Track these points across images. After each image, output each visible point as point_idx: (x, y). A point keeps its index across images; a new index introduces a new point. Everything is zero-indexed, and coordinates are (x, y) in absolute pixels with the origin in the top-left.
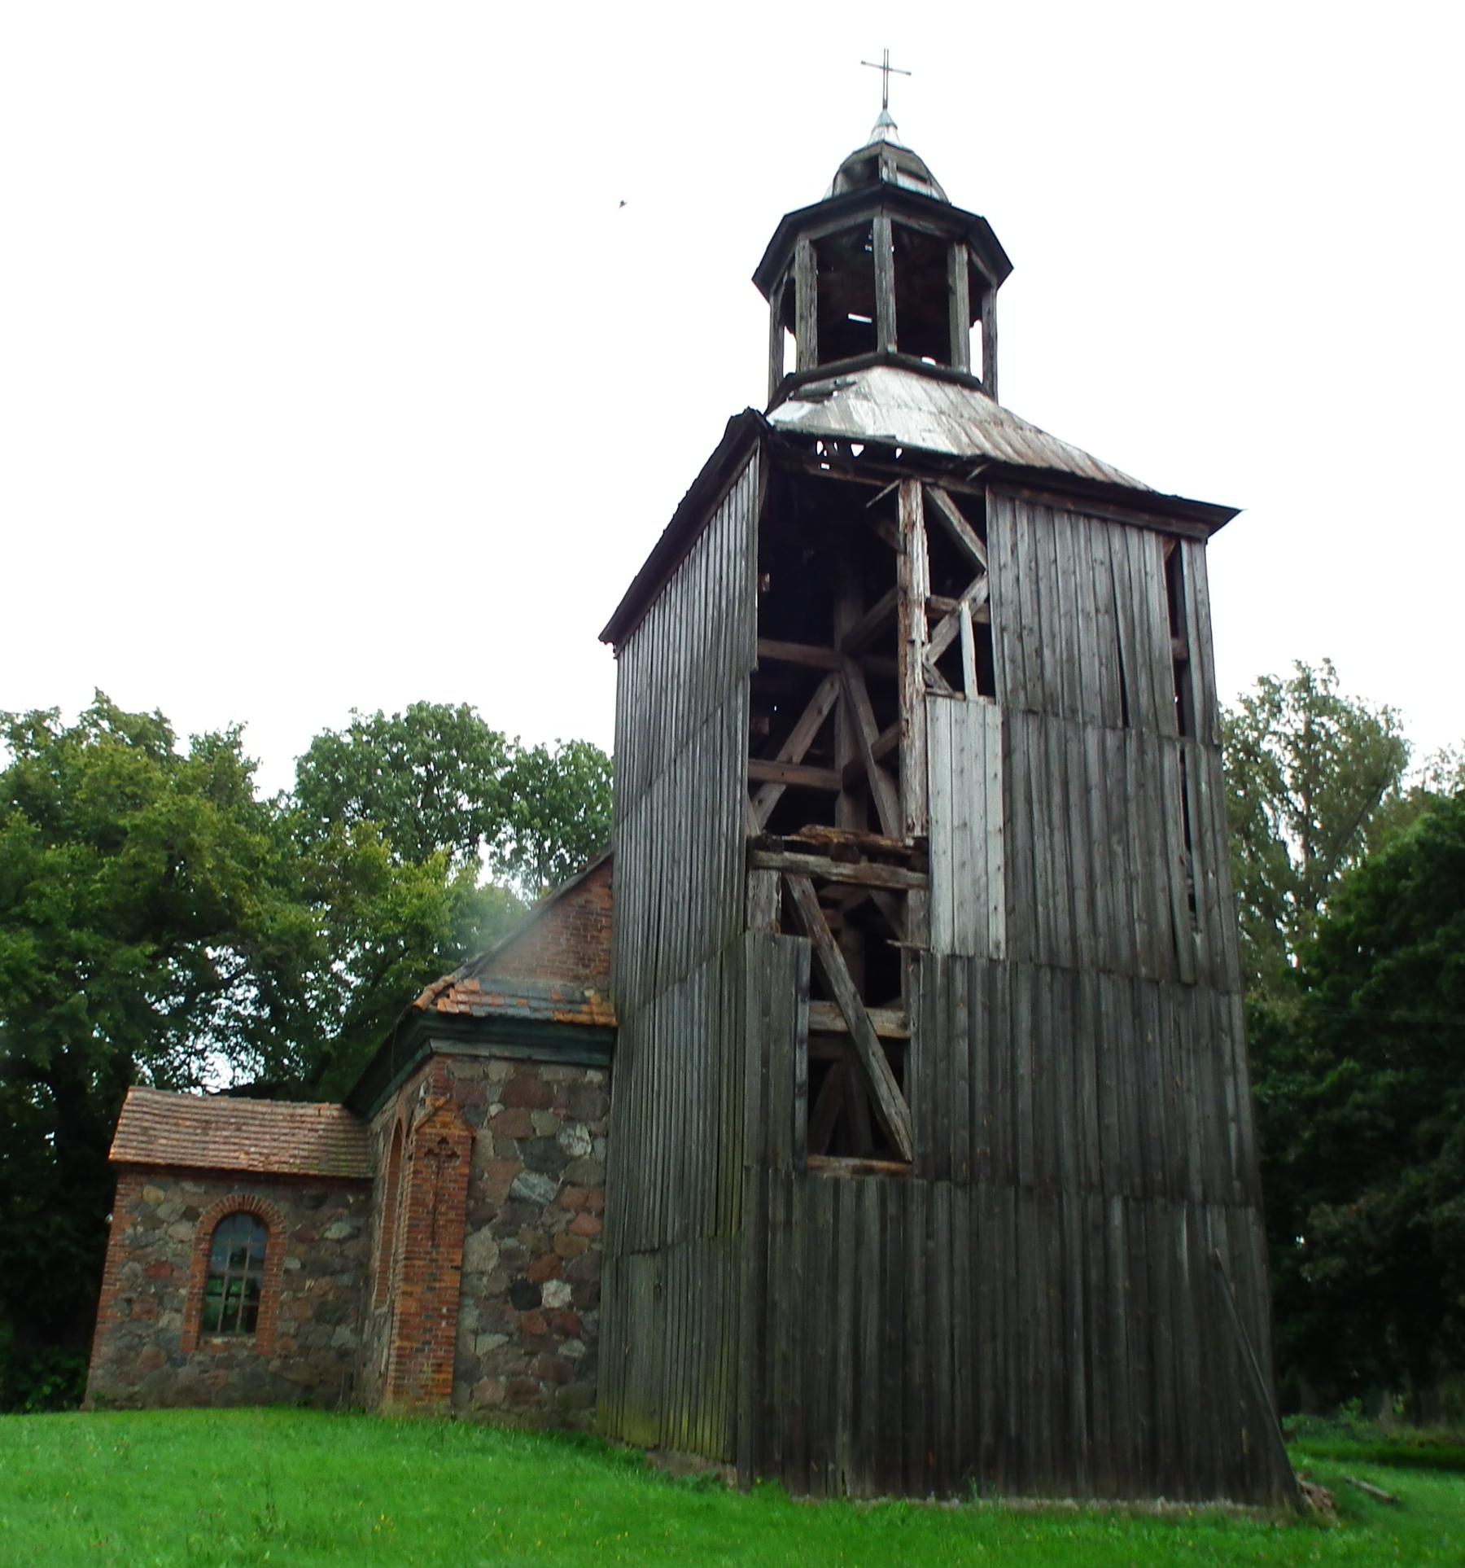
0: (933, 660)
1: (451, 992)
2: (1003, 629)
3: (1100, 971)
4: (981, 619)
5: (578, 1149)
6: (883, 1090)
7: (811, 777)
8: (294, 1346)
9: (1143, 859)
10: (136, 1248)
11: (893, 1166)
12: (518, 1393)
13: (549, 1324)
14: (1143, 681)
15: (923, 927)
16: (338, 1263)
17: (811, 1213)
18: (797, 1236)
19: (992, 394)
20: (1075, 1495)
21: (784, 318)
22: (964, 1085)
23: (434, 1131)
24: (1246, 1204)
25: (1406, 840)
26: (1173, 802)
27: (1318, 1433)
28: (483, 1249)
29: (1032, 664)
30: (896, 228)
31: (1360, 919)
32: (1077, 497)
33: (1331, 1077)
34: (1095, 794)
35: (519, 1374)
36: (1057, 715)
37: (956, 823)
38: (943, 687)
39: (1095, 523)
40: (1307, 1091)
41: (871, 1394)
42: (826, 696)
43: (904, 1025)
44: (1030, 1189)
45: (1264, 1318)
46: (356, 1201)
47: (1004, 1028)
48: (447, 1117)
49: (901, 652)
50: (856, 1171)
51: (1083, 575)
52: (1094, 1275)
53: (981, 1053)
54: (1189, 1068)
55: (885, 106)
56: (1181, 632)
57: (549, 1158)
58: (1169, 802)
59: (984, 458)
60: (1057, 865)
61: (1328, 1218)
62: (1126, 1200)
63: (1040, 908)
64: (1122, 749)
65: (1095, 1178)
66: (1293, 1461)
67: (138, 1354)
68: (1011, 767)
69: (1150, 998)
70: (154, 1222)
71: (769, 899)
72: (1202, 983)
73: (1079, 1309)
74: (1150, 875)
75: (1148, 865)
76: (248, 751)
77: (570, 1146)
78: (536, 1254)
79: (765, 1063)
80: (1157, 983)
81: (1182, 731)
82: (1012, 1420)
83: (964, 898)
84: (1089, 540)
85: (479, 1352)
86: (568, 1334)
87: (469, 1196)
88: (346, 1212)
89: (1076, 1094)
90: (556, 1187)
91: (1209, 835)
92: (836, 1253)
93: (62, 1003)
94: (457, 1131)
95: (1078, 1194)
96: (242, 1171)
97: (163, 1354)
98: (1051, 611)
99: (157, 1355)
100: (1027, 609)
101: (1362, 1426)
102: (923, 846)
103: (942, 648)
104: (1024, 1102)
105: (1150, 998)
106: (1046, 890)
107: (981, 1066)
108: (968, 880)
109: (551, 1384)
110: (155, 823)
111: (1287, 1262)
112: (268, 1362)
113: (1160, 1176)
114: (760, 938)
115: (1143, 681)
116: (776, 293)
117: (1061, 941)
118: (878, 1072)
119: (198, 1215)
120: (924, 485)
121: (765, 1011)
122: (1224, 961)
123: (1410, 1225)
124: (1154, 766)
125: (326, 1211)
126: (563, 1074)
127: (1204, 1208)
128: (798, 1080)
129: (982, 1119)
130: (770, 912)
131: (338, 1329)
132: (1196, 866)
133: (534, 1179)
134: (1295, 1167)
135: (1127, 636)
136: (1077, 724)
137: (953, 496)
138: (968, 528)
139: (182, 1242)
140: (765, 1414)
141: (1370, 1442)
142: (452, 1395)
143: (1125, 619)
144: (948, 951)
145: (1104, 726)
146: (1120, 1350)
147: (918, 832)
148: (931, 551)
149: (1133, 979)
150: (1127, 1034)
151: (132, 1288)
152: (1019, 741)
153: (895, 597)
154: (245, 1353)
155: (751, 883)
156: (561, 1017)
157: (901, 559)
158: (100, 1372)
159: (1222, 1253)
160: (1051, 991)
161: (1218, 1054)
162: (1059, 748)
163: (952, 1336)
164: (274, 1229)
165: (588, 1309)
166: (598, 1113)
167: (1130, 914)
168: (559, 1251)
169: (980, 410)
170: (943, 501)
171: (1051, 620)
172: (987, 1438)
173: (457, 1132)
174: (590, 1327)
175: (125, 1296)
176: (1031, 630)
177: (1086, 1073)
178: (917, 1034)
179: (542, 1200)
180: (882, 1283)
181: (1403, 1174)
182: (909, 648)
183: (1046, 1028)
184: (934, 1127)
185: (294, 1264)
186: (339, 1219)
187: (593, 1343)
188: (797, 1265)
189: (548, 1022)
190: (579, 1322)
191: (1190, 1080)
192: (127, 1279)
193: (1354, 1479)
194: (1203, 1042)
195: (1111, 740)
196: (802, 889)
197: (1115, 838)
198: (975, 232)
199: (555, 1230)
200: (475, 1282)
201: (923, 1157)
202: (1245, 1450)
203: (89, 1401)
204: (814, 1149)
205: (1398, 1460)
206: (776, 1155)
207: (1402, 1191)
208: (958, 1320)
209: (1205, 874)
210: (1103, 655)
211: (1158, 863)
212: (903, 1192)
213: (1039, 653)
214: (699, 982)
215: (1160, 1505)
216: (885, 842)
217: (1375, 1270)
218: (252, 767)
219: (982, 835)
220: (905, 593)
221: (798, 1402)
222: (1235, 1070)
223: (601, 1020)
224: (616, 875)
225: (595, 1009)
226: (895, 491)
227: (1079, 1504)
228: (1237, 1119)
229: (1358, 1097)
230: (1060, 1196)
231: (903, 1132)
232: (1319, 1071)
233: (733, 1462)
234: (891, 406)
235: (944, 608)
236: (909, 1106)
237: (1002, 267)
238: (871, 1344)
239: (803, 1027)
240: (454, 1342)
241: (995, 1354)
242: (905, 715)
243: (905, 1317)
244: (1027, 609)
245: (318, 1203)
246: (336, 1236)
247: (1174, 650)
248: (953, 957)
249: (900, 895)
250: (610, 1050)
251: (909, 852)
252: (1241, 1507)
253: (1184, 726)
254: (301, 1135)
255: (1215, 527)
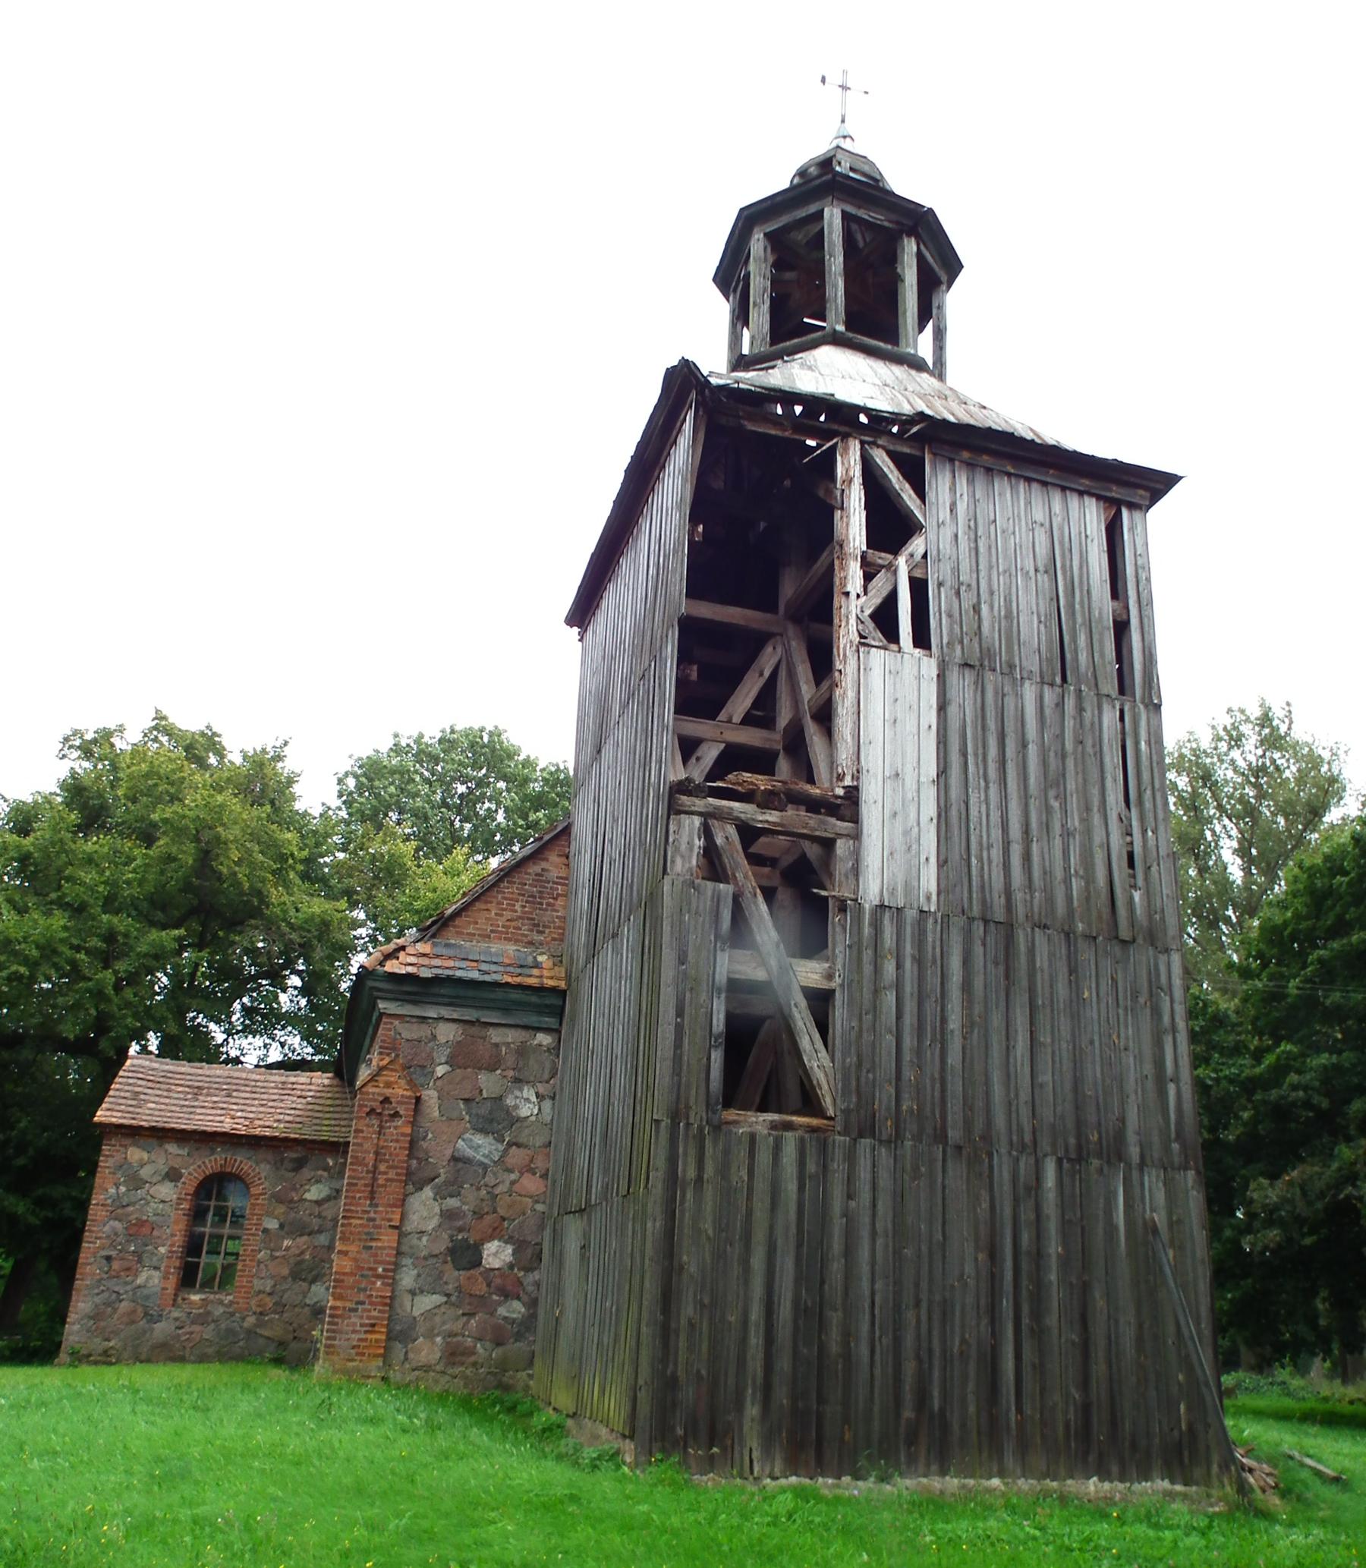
0: (868, 612)
1: (402, 954)
2: (940, 584)
3: (1035, 925)
4: (918, 574)
5: (525, 1111)
6: (805, 1043)
7: (751, 737)
8: (269, 1302)
9: (1080, 815)
10: (117, 1208)
11: (815, 1122)
12: (454, 1354)
13: (489, 1285)
14: (1082, 640)
15: (851, 876)
16: (315, 1223)
17: (724, 1171)
18: (709, 1192)
19: (941, 377)
20: (1001, 1474)
21: (741, 316)
22: (890, 1039)
23: (377, 1090)
24: (1186, 1169)
25: (1342, 840)
26: (1112, 759)
27: (1256, 1390)
28: (424, 1210)
29: (969, 616)
30: (846, 216)
31: (1297, 916)
32: (1014, 459)
33: (1270, 1059)
34: (1032, 750)
35: (456, 1335)
36: (994, 670)
37: (887, 774)
38: (877, 637)
39: (1035, 486)
40: (1247, 1072)
41: (784, 1364)
42: (768, 659)
43: (830, 977)
44: (959, 1148)
45: (1203, 1286)
46: (335, 1164)
47: (933, 980)
48: (391, 1076)
49: (836, 605)
50: (774, 1126)
51: (1022, 535)
52: (1025, 1238)
53: (910, 1007)
54: (1126, 1027)
55: (843, 121)
56: (1121, 597)
57: (495, 1119)
58: (1107, 760)
59: (921, 416)
60: (992, 818)
61: (1265, 1192)
62: (1059, 1161)
63: (974, 861)
64: (1060, 705)
65: (1028, 1138)
66: (1232, 1434)
67: (115, 1310)
68: (945, 720)
69: (1086, 954)
70: (136, 1182)
71: (690, 844)
72: (1140, 940)
73: (1009, 1275)
74: (1088, 832)
75: (1086, 821)
76: (288, 766)
77: (516, 1107)
78: (478, 1215)
79: (680, 1013)
80: (1095, 938)
81: (1122, 691)
82: (936, 1393)
83: (894, 851)
84: (1028, 503)
85: (416, 1313)
86: (506, 1295)
87: (410, 1156)
88: (325, 1174)
89: (1008, 1050)
90: (501, 1147)
91: (1149, 792)
92: (749, 1213)
93: (90, 979)
94: (400, 1091)
95: (1010, 1153)
96: (225, 1134)
97: (140, 1310)
98: (991, 567)
99: (134, 1311)
100: (965, 566)
101: (1296, 1382)
102: (853, 795)
103: (878, 601)
104: (954, 1058)
105: (1086, 954)
106: (981, 844)
107: (909, 1020)
108: (899, 829)
109: (488, 1344)
110: (184, 817)
111: (1228, 1233)
112: (243, 1319)
113: (1096, 1136)
114: (678, 883)
115: (1082, 640)
116: (735, 291)
117: (996, 895)
118: (800, 1024)
119: (181, 1176)
120: (862, 443)
121: (682, 960)
122: (1163, 919)
123: (1342, 1196)
124: (1092, 724)
125: (306, 1173)
126: (512, 1036)
127: (1141, 1171)
128: (715, 1030)
129: (909, 1074)
130: (690, 857)
131: (313, 1288)
132: (1135, 823)
133: (479, 1139)
134: (1234, 1143)
135: (1066, 596)
136: (1014, 679)
137: (892, 455)
138: (907, 486)
139: (163, 1201)
140: (667, 1385)
141: (1304, 1399)
142: (384, 1356)
143: (1065, 579)
144: (877, 902)
145: (1043, 683)
146: (1052, 1320)
147: (848, 781)
148: (868, 507)
149: (1068, 934)
150: (1062, 991)
151: (112, 1246)
152: (953, 693)
153: (832, 553)
154: (221, 1310)
155: (672, 828)
156: (510, 980)
157: (838, 514)
158: (76, 1327)
159: (1160, 1218)
160: (984, 945)
161: (1156, 1012)
162: (996, 701)
163: (873, 1303)
164: (253, 1191)
165: (528, 1269)
166: (546, 1076)
167: (1066, 869)
168: (501, 1212)
169: (925, 386)
170: (881, 458)
171: (990, 579)
172: (908, 1413)
173: (401, 1092)
174: (530, 1288)
175: (104, 1253)
176: (969, 586)
177: (1020, 1029)
178: (842, 985)
179: (486, 1161)
180: (799, 1246)
181: (1336, 1151)
182: (843, 599)
183: (978, 983)
184: (858, 1080)
185: (272, 1224)
186: (318, 1181)
187: (533, 1304)
188: (708, 1226)
189: (496, 984)
190: (520, 1282)
191: (1127, 1038)
192: (108, 1237)
193: (1296, 1454)
194: (1142, 1000)
195: (1050, 696)
196: (726, 835)
197: (1052, 793)
198: (921, 223)
199: (497, 1191)
200: (415, 1242)
201: (846, 1112)
202: (1184, 1427)
203: (63, 1356)
204: (728, 1103)
205: (1332, 1420)
206: (688, 1107)
207: (1335, 1165)
208: (878, 1286)
209: (1144, 832)
210: (1042, 613)
211: (1097, 819)
212: (824, 1148)
213: (977, 609)
214: (629, 935)
215: (1093, 1485)
216: (815, 791)
217: (1308, 1241)
218: (290, 782)
219: (915, 787)
220: (841, 546)
221: (704, 1372)
222: (1174, 1029)
223: (550, 983)
224: (573, 843)
225: (546, 973)
226: (834, 448)
227: (1006, 1484)
228: (1176, 1079)
229: (1293, 1078)
230: (990, 1155)
231: (825, 1087)
232: (1258, 1056)
233: (632, 1437)
234: (835, 373)
235: (880, 561)
236: (833, 1062)
237: (953, 266)
238: (785, 1311)
239: (721, 977)
240: (391, 1302)
241: (918, 1321)
242: (838, 665)
243: (822, 1282)
244: (965, 566)
245: (299, 1165)
246: (314, 1198)
247: (1114, 611)
248: (882, 907)
249: (828, 844)
250: (559, 1013)
251: (839, 801)
252: (1179, 1488)
253: (1124, 686)
254: (289, 1102)
255: (1156, 496)
